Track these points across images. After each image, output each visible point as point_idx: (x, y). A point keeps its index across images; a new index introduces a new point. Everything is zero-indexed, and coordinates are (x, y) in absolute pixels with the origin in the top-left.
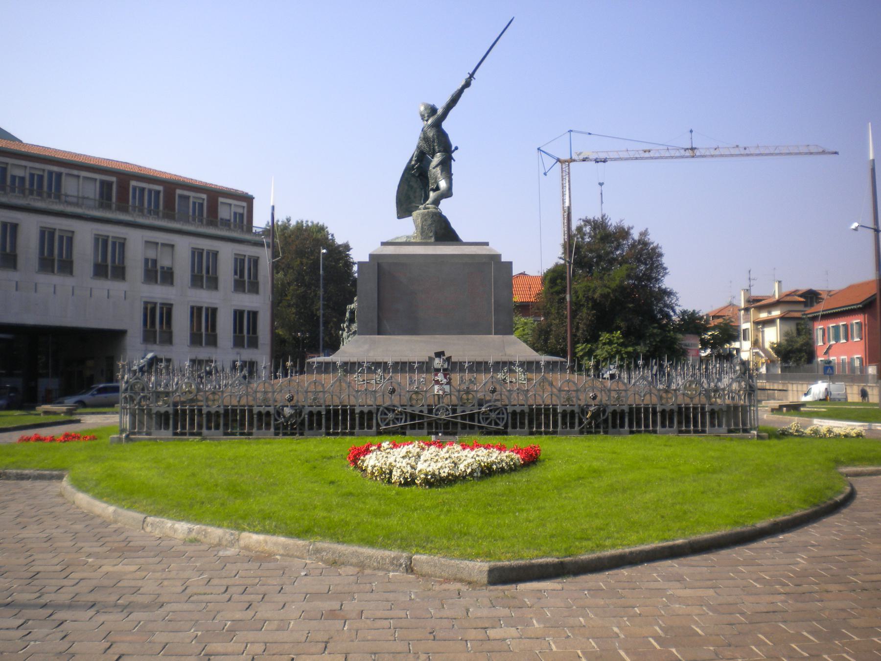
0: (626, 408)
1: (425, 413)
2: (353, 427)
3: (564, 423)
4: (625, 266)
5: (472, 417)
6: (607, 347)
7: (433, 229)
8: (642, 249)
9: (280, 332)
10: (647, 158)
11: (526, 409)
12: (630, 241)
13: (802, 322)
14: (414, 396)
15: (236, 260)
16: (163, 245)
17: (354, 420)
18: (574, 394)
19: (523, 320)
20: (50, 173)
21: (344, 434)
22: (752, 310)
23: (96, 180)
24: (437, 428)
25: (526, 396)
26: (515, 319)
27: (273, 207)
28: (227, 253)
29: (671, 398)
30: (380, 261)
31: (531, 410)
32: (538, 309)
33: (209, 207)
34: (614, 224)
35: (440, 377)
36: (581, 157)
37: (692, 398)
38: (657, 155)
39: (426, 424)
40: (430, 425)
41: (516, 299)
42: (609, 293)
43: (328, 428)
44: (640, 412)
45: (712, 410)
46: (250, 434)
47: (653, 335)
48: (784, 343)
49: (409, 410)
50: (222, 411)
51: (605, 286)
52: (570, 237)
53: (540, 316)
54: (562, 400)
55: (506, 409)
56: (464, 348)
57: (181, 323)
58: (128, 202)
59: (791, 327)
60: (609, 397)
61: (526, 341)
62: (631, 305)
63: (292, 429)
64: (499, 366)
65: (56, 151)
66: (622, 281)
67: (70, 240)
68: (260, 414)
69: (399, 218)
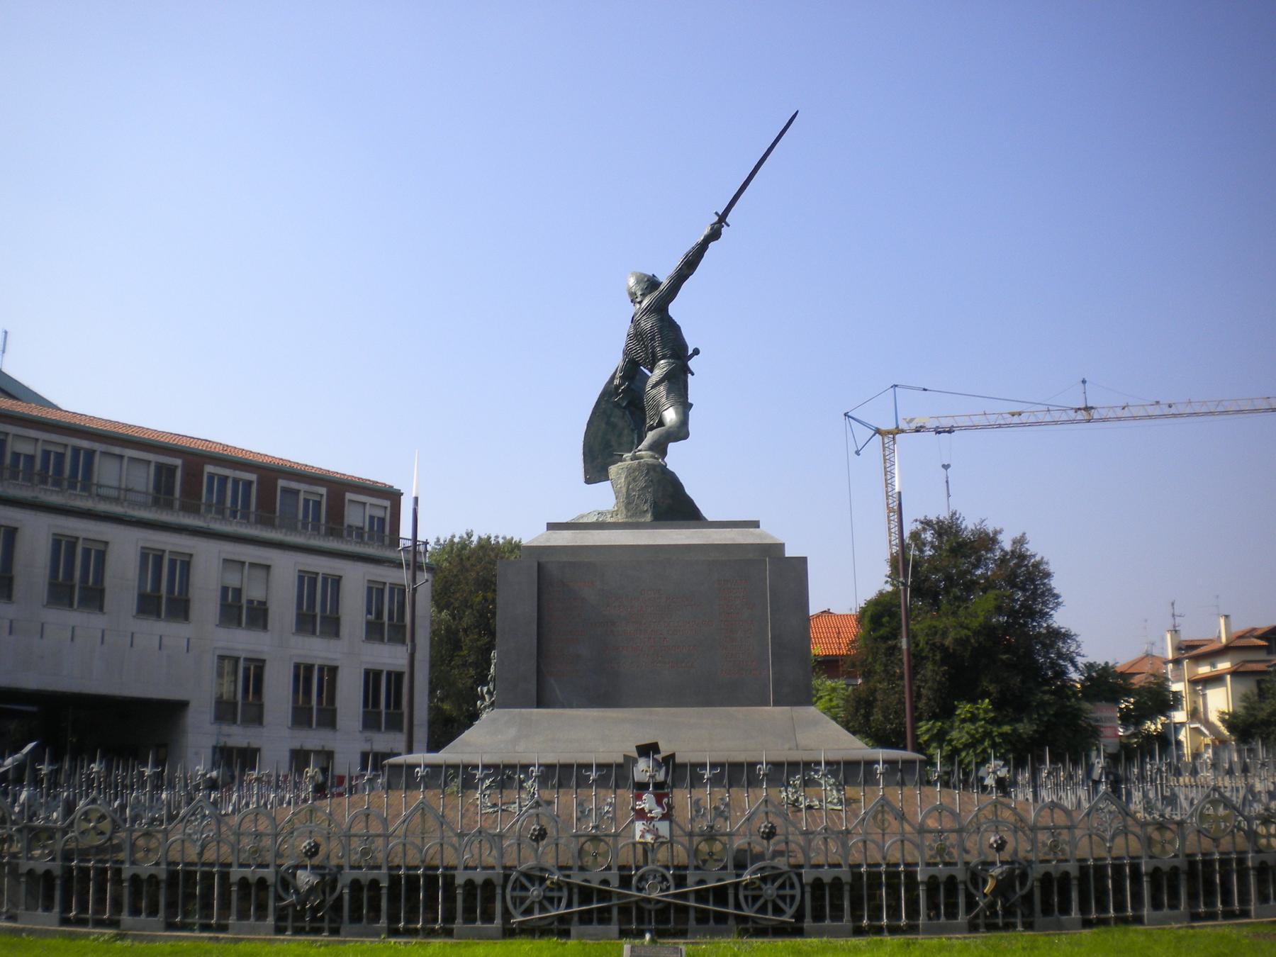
0: (1072, 868)
1: (614, 886)
2: (450, 917)
3: (933, 905)
4: (991, 594)
5: (720, 894)
6: (969, 726)
7: (649, 496)
8: (1018, 566)
9: (446, 706)
10: (1017, 425)
11: (845, 874)
12: (998, 553)
13: (1267, 678)
14: (589, 847)
15: (370, 590)
16: (252, 565)
17: (454, 900)
18: (953, 838)
19: (829, 683)
20: (76, 450)
21: (431, 933)
22: (1185, 662)
23: (149, 462)
24: (640, 920)
25: (844, 845)
26: (816, 682)
27: (416, 499)
28: (355, 578)
29: (1171, 842)
30: (544, 559)
31: (857, 876)
32: (854, 665)
33: (329, 507)
34: (971, 527)
35: (647, 802)
36: (913, 425)
37: (1216, 840)
38: (1032, 419)
39: (615, 912)
40: (624, 911)
41: (817, 650)
42: (968, 638)
43: (394, 918)
44: (1105, 877)
45: (1263, 863)
46: (223, 928)
47: (1043, 704)
48: (1241, 711)
49: (577, 879)
50: (163, 876)
51: (962, 626)
52: (904, 547)
53: (855, 677)
54: (928, 853)
55: (800, 876)
56: (700, 734)
57: (278, 691)
58: (200, 499)
59: (1249, 686)
60: (1033, 842)
61: (835, 718)
62: (1004, 657)
63: (314, 919)
64: (781, 771)
65: (92, 419)
66: (988, 619)
67: (102, 556)
68: (244, 883)
69: (588, 481)
